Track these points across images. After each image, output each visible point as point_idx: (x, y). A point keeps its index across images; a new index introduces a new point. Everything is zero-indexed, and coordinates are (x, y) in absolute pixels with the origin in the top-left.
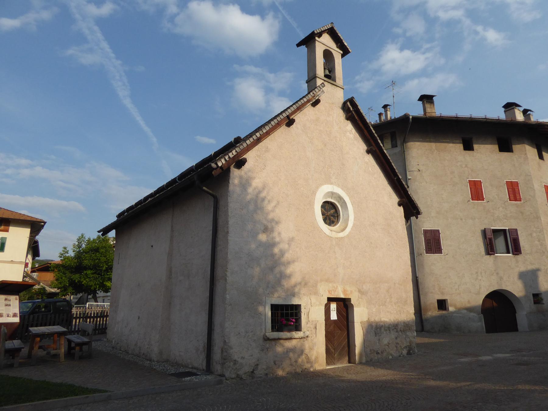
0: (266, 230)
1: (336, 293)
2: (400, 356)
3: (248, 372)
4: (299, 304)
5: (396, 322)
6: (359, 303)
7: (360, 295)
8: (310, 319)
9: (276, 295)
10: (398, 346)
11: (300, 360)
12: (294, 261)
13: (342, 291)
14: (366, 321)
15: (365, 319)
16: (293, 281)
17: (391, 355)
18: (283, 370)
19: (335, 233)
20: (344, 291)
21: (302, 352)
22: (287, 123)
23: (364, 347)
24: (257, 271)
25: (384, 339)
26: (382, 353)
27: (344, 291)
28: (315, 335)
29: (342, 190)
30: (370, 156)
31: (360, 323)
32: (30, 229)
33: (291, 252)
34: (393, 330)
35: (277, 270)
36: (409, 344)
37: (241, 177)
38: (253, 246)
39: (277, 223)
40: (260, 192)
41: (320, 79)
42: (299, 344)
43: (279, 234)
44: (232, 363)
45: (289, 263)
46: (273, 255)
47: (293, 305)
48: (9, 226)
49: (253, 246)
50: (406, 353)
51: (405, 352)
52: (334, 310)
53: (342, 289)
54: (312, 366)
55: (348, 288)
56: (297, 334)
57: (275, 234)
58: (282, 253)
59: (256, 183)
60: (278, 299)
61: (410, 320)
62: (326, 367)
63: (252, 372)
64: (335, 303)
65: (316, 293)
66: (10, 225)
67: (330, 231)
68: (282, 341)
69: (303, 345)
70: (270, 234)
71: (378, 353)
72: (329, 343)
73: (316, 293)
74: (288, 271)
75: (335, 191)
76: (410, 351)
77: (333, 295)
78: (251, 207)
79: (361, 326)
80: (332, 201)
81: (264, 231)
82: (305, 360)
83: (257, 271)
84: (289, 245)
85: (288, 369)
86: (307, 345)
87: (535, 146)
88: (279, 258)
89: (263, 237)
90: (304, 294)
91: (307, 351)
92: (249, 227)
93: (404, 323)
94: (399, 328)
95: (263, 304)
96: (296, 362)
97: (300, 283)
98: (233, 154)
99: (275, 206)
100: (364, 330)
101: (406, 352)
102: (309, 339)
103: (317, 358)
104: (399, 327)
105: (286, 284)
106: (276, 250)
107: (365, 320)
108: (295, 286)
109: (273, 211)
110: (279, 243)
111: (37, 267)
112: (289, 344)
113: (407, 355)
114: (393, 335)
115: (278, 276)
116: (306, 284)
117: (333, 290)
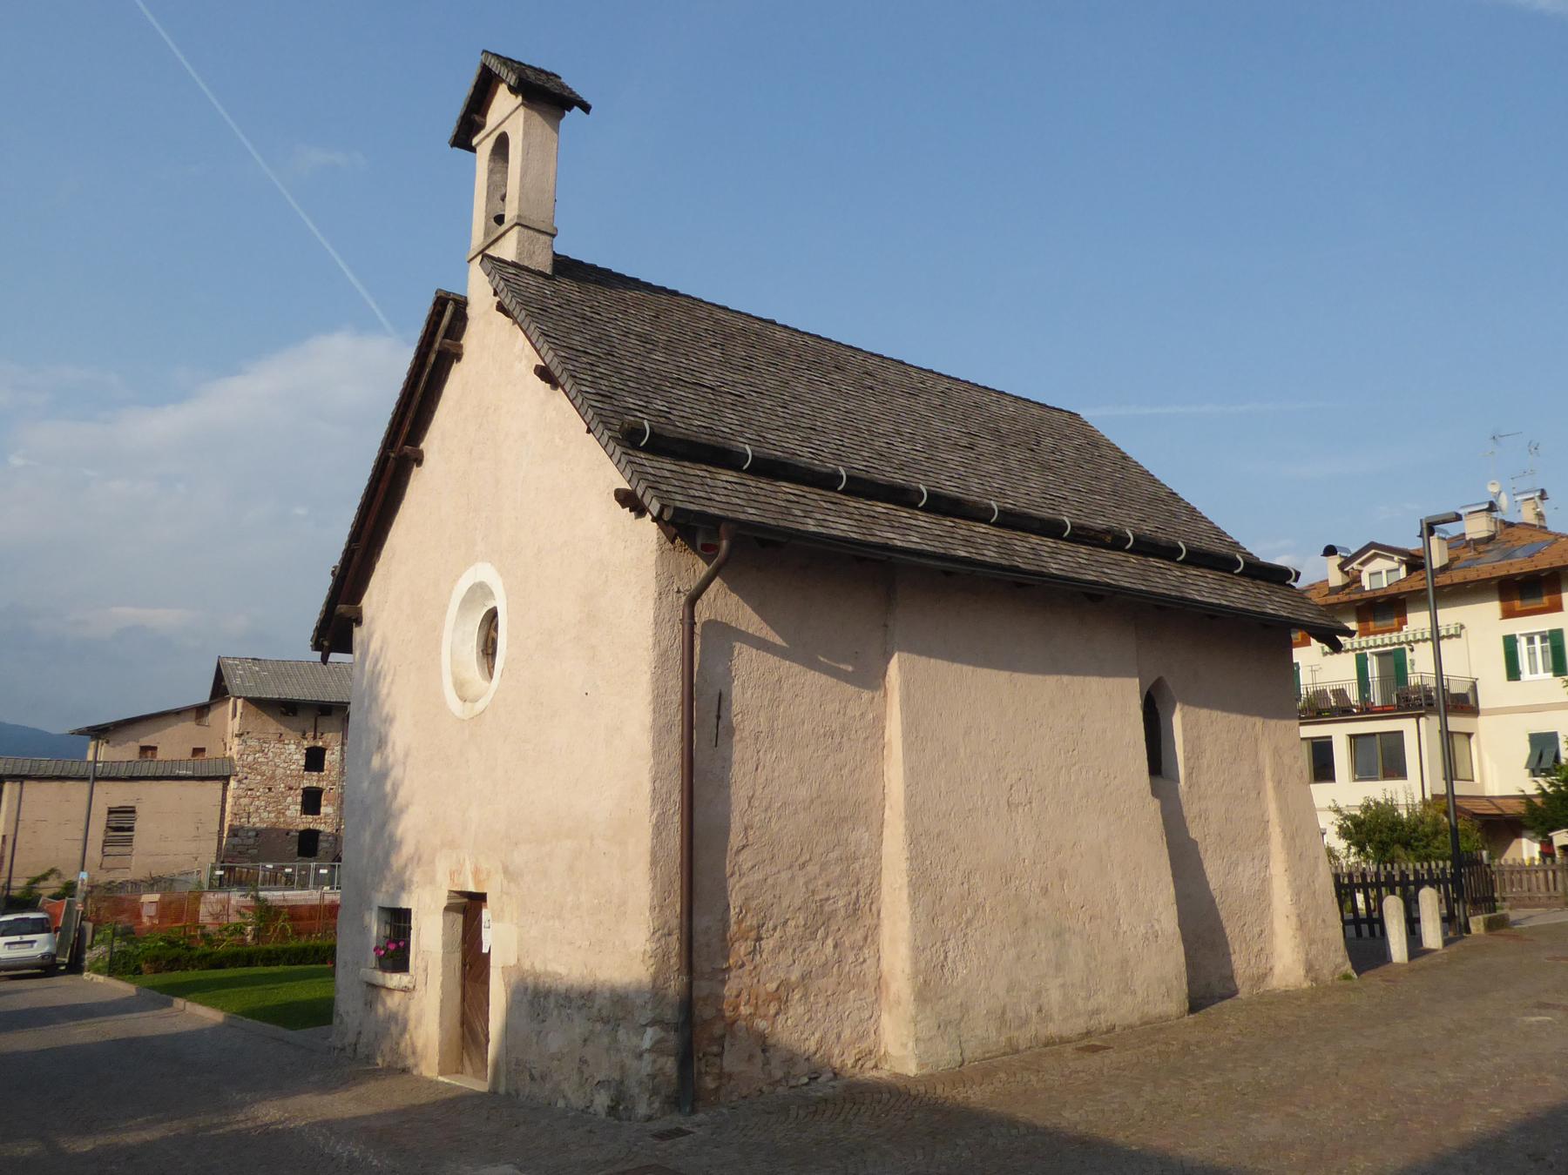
5: (588, 983)
7: (505, 882)
12: (407, 807)
22: (76, 887)
25: (551, 1034)
26: (543, 1078)
31: (500, 970)
32: (1137, 680)
47: (401, 909)
48: (1560, 592)
50: (606, 1105)
51: (602, 1100)
60: (381, 899)
61: (630, 983)
66: (1408, 611)
93: (613, 990)
94: (597, 1006)
101: (607, 1102)
103: (425, 1046)
104: (598, 1002)
111: (289, 867)
113: (609, 1114)
114: (579, 1027)
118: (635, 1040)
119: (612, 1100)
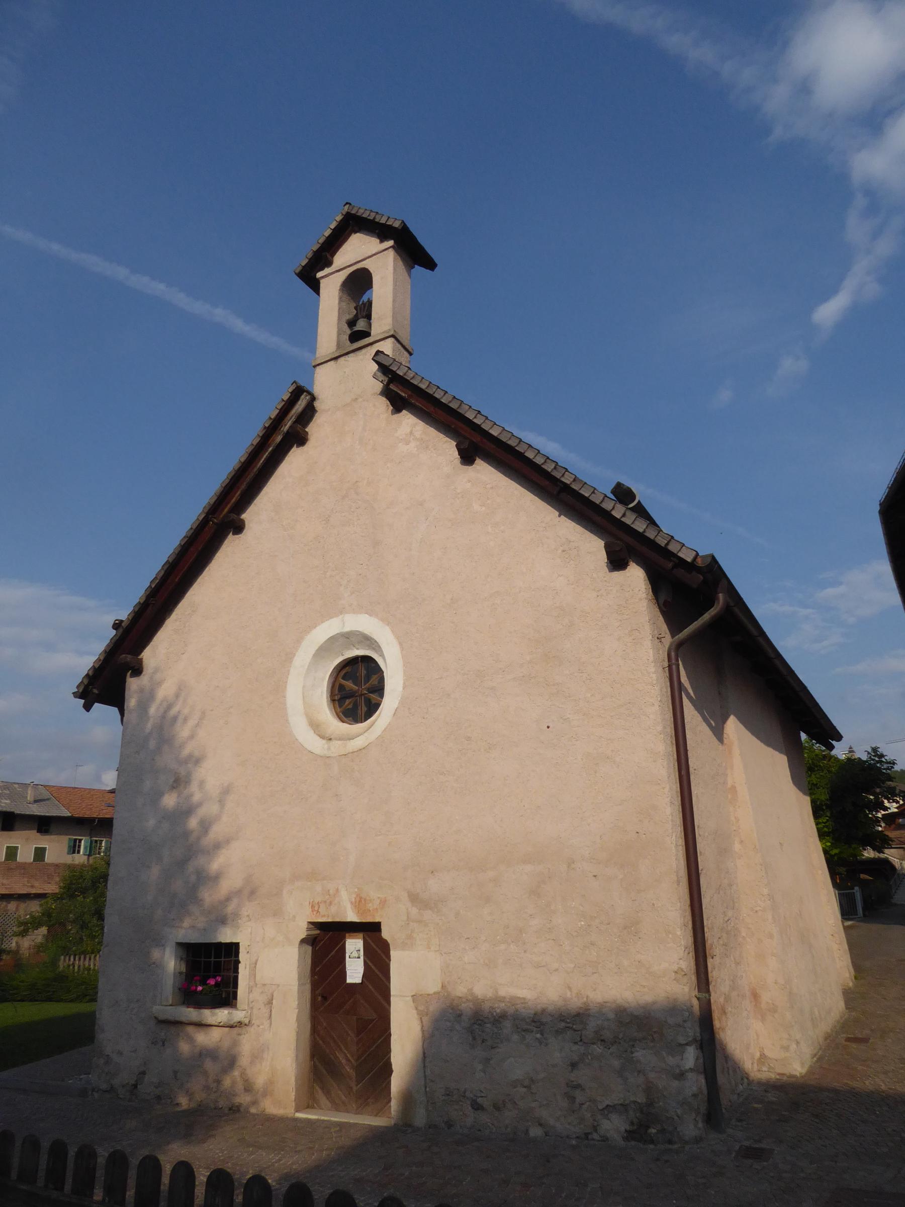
0: (179, 782)
1: (333, 909)
2: (587, 1139)
3: (128, 1084)
4: (234, 941)
6: (410, 937)
8: (258, 978)
9: (187, 923)
10: (580, 1097)
11: (227, 1082)
12: (228, 841)
13: (352, 903)
14: (435, 993)
15: (432, 986)
16: (226, 886)
17: (541, 1125)
18: (190, 1095)
19: (339, 742)
20: (360, 903)
21: (231, 1062)
23: (425, 1076)
24: (155, 872)
27: (360, 901)
28: (267, 1023)
29: (371, 615)
30: (478, 467)
31: (410, 999)
33: (224, 819)
34: (558, 1032)
35: (191, 867)
36: (641, 1099)
37: (141, 690)
38: (151, 823)
39: (198, 761)
40: (170, 707)
41: (325, 364)
42: (226, 1044)
43: (202, 784)
44: (102, 1061)
45: (217, 846)
46: (186, 834)
47: (220, 944)
49: (151, 823)
50: (623, 1129)
52: (355, 954)
53: (354, 896)
54: (255, 1103)
55: (373, 894)
56: (214, 1015)
57: (194, 787)
58: (206, 826)
59: (165, 691)
62: (297, 1111)
63: (135, 1086)
64: (361, 935)
65: (277, 913)
67: (324, 742)
68: (190, 1029)
69: (235, 1043)
70: (185, 788)
71: (477, 1107)
72: (341, 1049)
73: (277, 913)
74: (215, 866)
75: (347, 629)
76: (648, 1127)
77: (324, 916)
78: (152, 744)
79: (416, 1009)
80: (340, 659)
81: (175, 785)
82: (240, 1086)
83: (155, 872)
84: (221, 802)
85: (200, 1096)
86: (247, 1044)
87: (376, 236)
88: (199, 839)
89: (170, 801)
90: (248, 916)
91: (244, 1061)
92: (148, 784)
95: (159, 942)
96: (218, 1082)
97: (239, 892)
98: (624, 515)
99: (197, 725)
100: (424, 1023)
102: (252, 1030)
105: (208, 896)
106: (193, 823)
107: (431, 992)
108: (228, 899)
109: (192, 737)
110: (200, 805)
112: (203, 1039)
113: (626, 1139)
115: (193, 878)
116: (253, 893)
117: (325, 902)
118: (671, 1060)
119: (632, 1123)
